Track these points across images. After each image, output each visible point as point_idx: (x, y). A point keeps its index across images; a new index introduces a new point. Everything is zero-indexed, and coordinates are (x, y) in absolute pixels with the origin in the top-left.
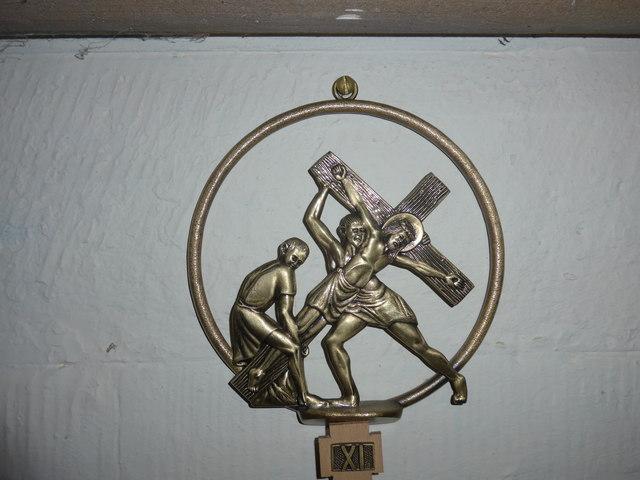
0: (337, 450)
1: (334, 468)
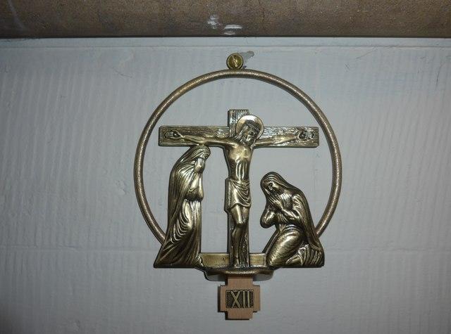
0: (228, 294)
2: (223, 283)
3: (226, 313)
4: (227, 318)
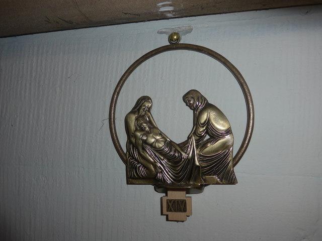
0: (169, 201)
1: (169, 209)
2: (164, 194)
3: (167, 216)
4: (167, 220)
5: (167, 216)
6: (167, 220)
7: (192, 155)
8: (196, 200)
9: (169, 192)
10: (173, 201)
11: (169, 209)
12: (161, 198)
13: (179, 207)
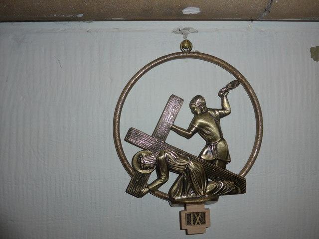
0: (189, 216)
1: (189, 223)
2: (183, 208)
3: (186, 230)
4: (187, 234)
5: (186, 230)
6: (173, 96)
7: (156, 186)
8: (214, 209)
9: (188, 207)
10: (196, 223)
11: (189, 223)
12: (180, 213)
13: (201, 219)
